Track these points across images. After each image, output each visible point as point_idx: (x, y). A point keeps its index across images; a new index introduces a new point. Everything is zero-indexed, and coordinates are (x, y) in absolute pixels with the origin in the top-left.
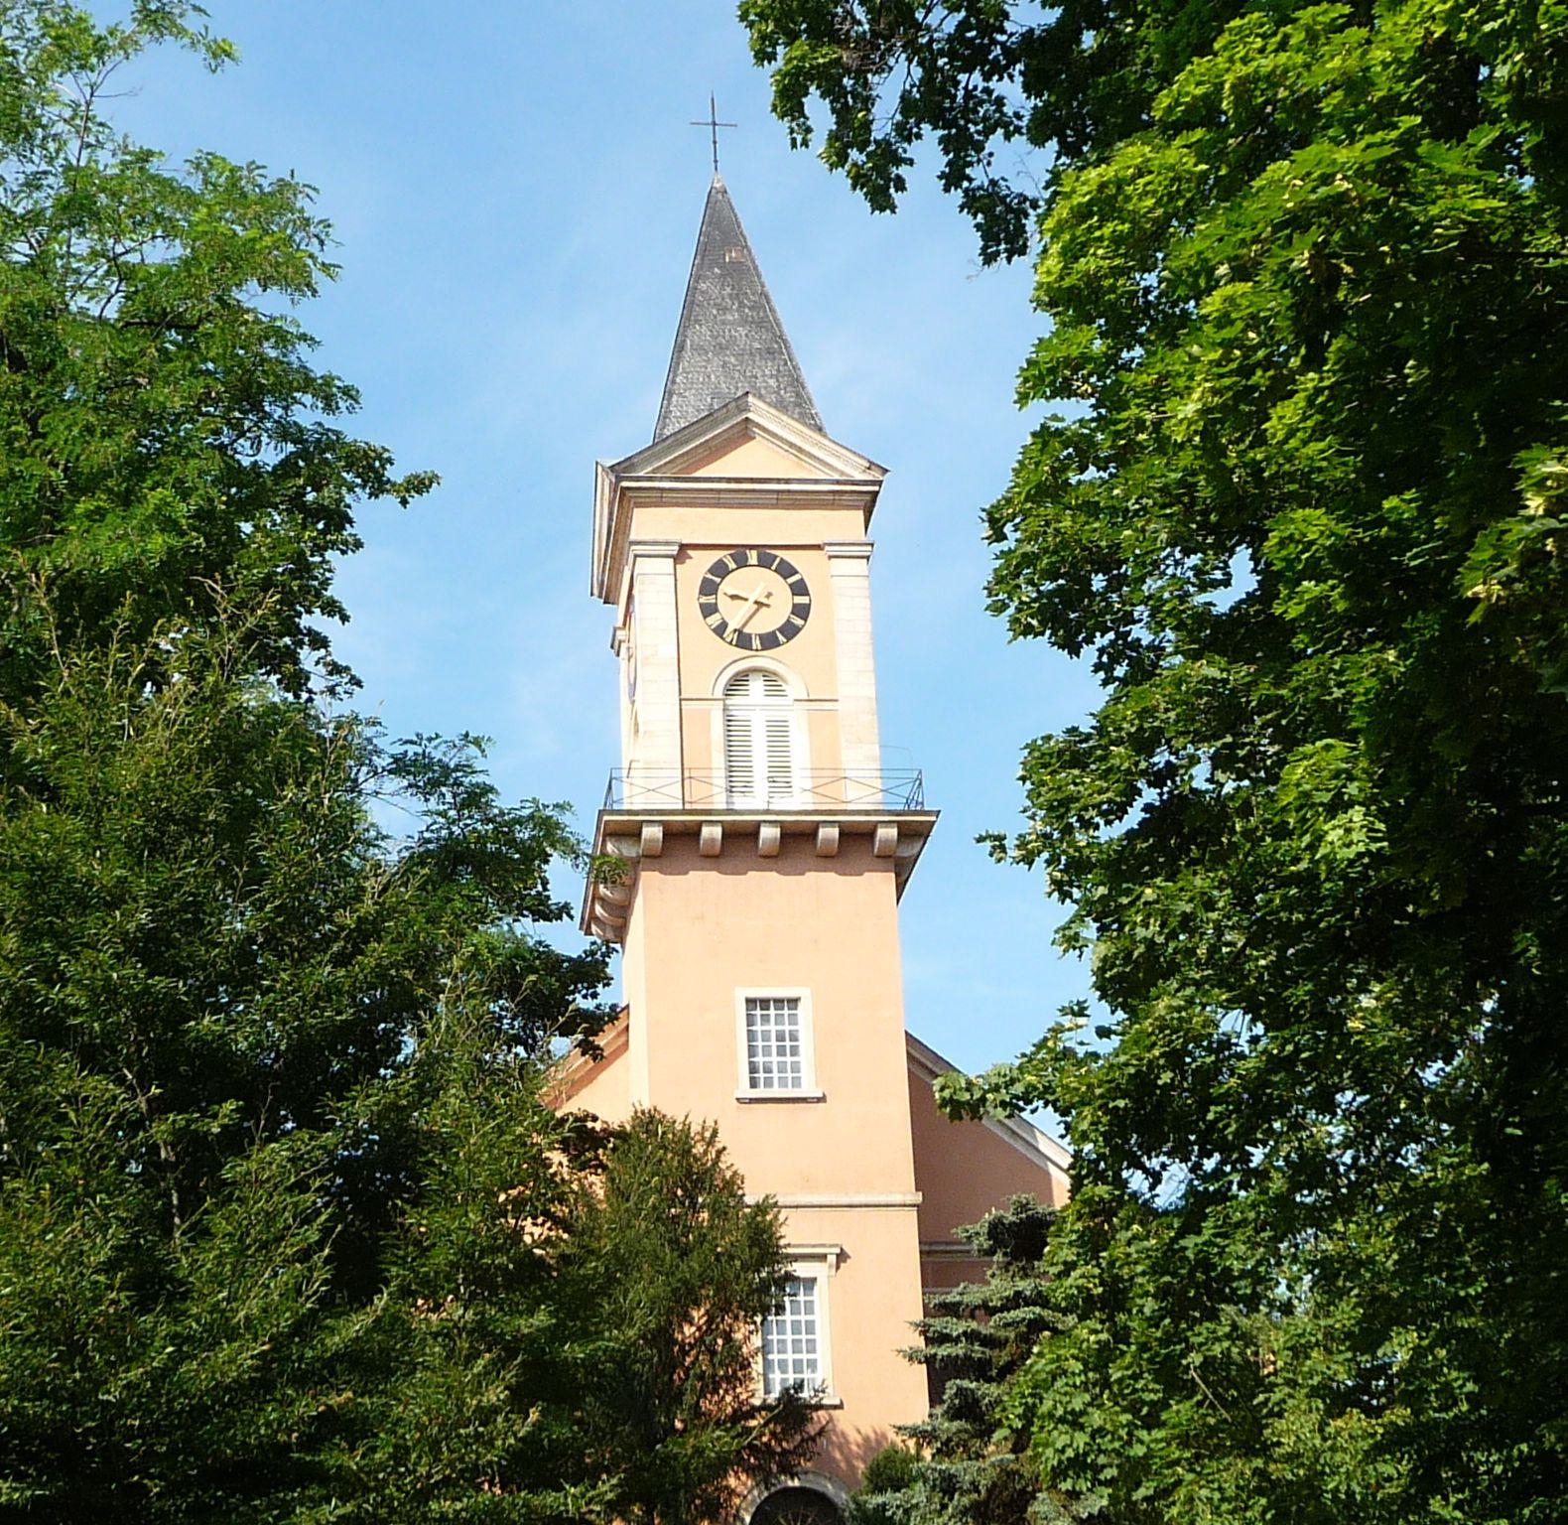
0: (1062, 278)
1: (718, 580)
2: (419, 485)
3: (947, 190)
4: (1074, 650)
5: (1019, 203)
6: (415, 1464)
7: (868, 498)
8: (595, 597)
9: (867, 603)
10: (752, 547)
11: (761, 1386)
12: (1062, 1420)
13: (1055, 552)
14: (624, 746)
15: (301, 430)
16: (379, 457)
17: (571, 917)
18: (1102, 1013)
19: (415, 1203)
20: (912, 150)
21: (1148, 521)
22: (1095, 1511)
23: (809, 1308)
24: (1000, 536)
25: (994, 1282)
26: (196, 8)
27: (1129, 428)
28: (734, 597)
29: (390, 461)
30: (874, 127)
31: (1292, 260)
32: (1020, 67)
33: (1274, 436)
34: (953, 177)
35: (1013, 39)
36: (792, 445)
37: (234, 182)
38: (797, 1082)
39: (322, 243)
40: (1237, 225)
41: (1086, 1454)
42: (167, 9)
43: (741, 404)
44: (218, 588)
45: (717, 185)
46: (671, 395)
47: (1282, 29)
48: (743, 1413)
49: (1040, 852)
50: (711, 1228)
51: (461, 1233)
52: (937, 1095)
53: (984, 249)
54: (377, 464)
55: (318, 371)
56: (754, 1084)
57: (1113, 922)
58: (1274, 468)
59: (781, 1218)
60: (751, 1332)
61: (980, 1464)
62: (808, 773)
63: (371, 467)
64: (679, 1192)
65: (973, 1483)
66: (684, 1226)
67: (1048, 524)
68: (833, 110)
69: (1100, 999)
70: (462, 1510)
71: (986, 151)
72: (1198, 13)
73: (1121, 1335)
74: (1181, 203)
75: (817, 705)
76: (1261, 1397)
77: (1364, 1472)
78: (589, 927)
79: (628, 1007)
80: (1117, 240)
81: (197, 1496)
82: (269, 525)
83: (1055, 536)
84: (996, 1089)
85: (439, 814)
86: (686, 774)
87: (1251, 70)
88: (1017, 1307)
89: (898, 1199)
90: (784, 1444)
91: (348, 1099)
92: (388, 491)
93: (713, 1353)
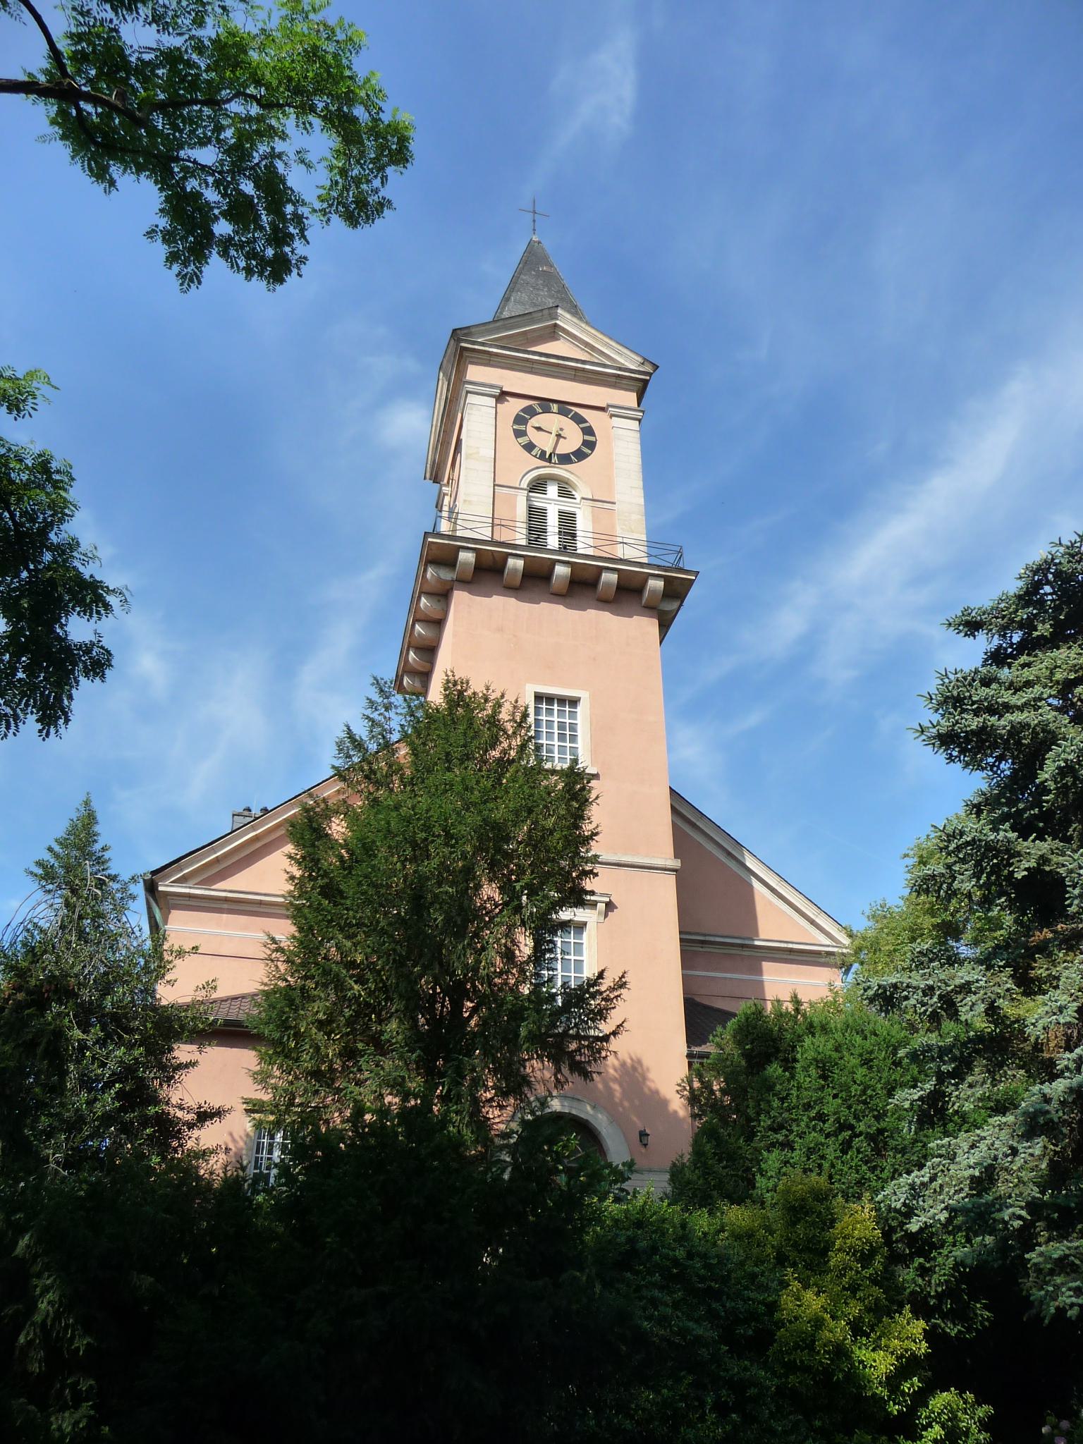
7: (640, 384)
28: (539, 429)
36: (587, 344)
43: (551, 312)
75: (599, 504)
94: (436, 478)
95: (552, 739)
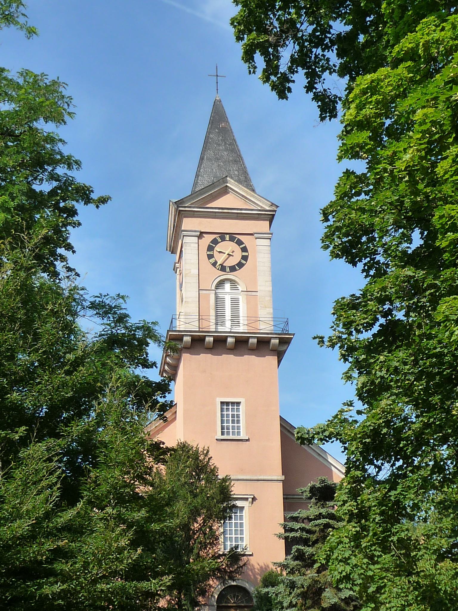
0: (356, 117)
1: (214, 245)
2: (103, 200)
3: (307, 92)
4: (355, 264)
5: (334, 98)
6: (92, 569)
7: (271, 216)
8: (168, 251)
9: (270, 256)
10: (227, 234)
11: (223, 546)
12: (341, 561)
13: (348, 227)
14: (177, 308)
15: (58, 176)
16: (88, 190)
17: (157, 367)
18: (359, 405)
19: (94, 467)
20: (294, 77)
21: (385, 215)
22: (347, 596)
23: (241, 518)
24: (326, 220)
25: (311, 509)
26: (23, 15)
27: (381, 171)
29: (92, 191)
30: (280, 67)
31: (452, 97)
32: (336, 47)
33: (439, 174)
34: (310, 87)
35: (334, 36)
36: (243, 196)
37: (36, 81)
38: (239, 433)
39: (68, 105)
40: (426, 94)
41: (350, 574)
42: (12, 14)
44: (26, 238)
45: (217, 99)
46: (198, 177)
47: (442, 24)
48: (216, 557)
49: (337, 344)
50: (206, 487)
51: (112, 479)
52: (296, 435)
53: (321, 115)
54: (87, 192)
55: (66, 153)
56: (223, 434)
57: (364, 371)
58: (434, 195)
59: (232, 484)
60: (219, 526)
61: (305, 577)
62: (246, 318)
63: (85, 193)
64: (194, 474)
65: (302, 585)
66: (196, 486)
67: (346, 215)
68: (265, 61)
69: (359, 400)
70: (110, 588)
71: (323, 78)
72: (408, 21)
73: (364, 528)
74: (402, 90)
76: (415, 553)
77: (451, 583)
78: (162, 374)
79: (176, 404)
80: (377, 102)
81: (5, 581)
82: (46, 216)
83: (349, 220)
84: (318, 433)
85: (107, 324)
86: (201, 318)
87: (431, 38)
88: (320, 519)
89: (275, 478)
90: (231, 569)
91: (69, 427)
92: (91, 202)
93: (205, 534)
94: (173, 252)
95: (229, 423)
